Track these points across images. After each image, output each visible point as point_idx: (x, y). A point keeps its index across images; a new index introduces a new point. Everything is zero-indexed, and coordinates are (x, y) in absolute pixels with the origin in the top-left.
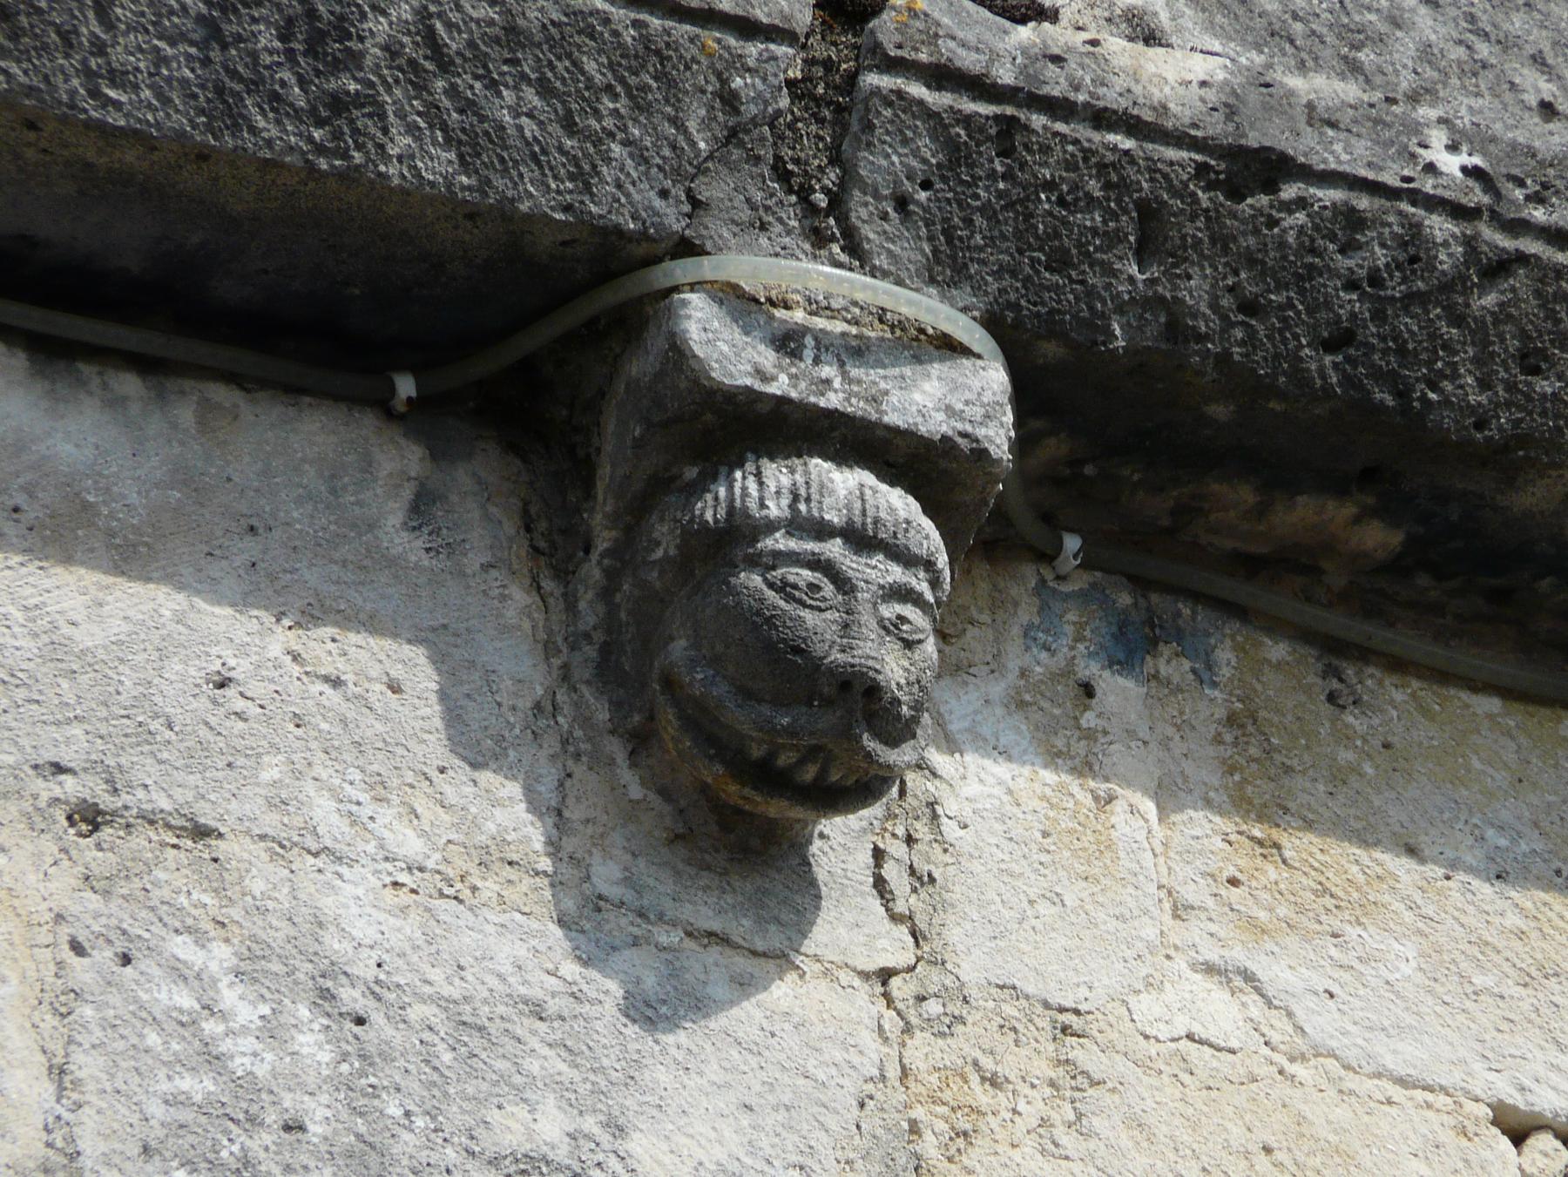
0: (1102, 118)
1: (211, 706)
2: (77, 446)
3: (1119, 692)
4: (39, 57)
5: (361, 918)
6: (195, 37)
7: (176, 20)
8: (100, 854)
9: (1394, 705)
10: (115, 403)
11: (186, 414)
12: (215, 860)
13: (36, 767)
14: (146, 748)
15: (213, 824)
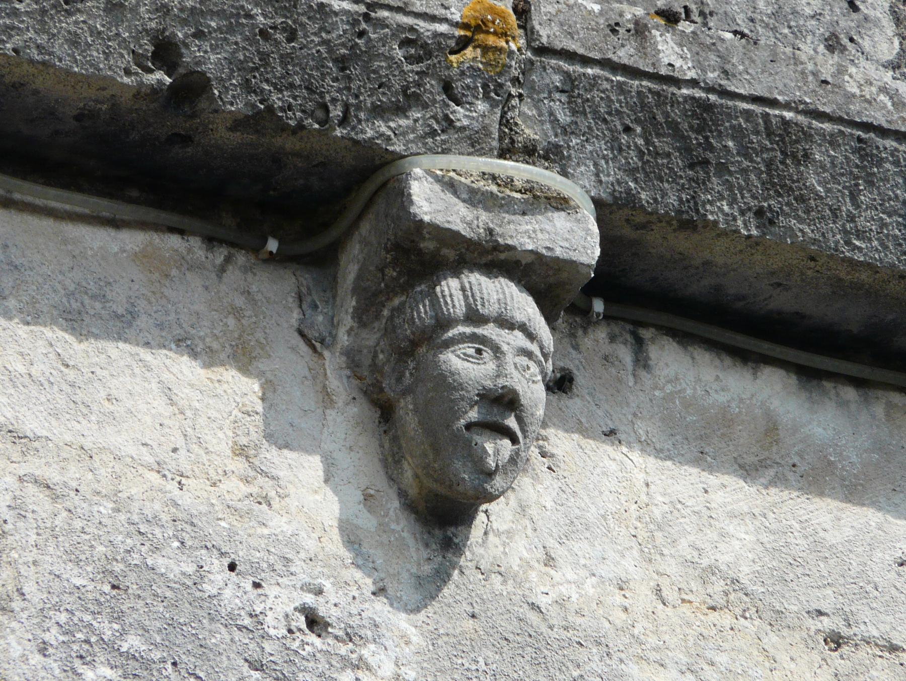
1: (897, 577)
2: (824, 429)
4: (820, 223)
6: (902, 212)
7: (892, 203)
8: (843, 661)
10: (843, 404)
11: (879, 410)
12: (902, 665)
13: (808, 612)
14: (865, 601)
15: (900, 644)
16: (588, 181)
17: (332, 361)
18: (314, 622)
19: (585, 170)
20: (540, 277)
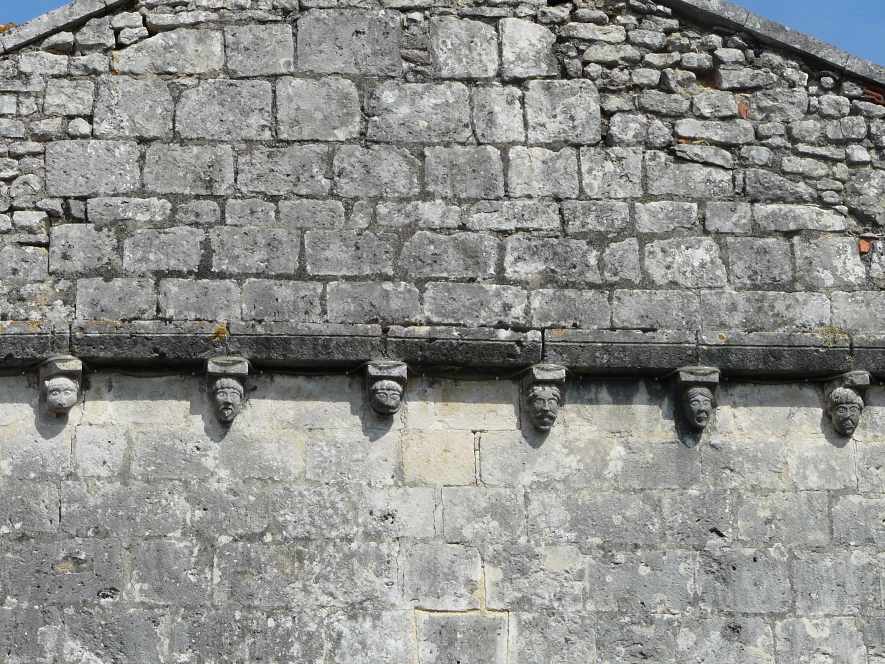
0: (414, 338)
3: (429, 390)
5: (340, 435)
9: (463, 384)
16: (246, 356)
17: (205, 395)
18: (198, 449)
19: (246, 355)
20: (239, 378)
